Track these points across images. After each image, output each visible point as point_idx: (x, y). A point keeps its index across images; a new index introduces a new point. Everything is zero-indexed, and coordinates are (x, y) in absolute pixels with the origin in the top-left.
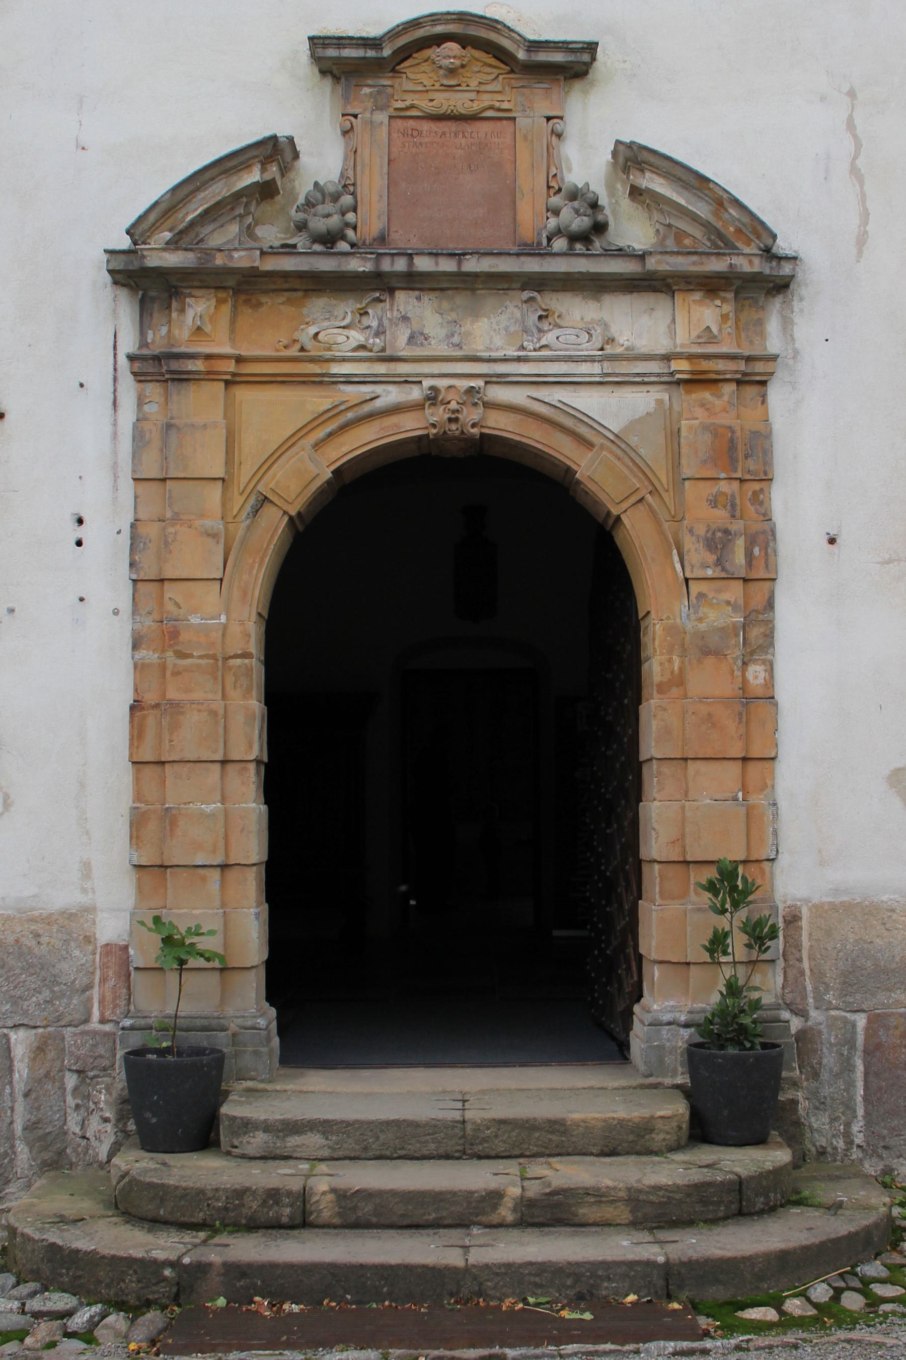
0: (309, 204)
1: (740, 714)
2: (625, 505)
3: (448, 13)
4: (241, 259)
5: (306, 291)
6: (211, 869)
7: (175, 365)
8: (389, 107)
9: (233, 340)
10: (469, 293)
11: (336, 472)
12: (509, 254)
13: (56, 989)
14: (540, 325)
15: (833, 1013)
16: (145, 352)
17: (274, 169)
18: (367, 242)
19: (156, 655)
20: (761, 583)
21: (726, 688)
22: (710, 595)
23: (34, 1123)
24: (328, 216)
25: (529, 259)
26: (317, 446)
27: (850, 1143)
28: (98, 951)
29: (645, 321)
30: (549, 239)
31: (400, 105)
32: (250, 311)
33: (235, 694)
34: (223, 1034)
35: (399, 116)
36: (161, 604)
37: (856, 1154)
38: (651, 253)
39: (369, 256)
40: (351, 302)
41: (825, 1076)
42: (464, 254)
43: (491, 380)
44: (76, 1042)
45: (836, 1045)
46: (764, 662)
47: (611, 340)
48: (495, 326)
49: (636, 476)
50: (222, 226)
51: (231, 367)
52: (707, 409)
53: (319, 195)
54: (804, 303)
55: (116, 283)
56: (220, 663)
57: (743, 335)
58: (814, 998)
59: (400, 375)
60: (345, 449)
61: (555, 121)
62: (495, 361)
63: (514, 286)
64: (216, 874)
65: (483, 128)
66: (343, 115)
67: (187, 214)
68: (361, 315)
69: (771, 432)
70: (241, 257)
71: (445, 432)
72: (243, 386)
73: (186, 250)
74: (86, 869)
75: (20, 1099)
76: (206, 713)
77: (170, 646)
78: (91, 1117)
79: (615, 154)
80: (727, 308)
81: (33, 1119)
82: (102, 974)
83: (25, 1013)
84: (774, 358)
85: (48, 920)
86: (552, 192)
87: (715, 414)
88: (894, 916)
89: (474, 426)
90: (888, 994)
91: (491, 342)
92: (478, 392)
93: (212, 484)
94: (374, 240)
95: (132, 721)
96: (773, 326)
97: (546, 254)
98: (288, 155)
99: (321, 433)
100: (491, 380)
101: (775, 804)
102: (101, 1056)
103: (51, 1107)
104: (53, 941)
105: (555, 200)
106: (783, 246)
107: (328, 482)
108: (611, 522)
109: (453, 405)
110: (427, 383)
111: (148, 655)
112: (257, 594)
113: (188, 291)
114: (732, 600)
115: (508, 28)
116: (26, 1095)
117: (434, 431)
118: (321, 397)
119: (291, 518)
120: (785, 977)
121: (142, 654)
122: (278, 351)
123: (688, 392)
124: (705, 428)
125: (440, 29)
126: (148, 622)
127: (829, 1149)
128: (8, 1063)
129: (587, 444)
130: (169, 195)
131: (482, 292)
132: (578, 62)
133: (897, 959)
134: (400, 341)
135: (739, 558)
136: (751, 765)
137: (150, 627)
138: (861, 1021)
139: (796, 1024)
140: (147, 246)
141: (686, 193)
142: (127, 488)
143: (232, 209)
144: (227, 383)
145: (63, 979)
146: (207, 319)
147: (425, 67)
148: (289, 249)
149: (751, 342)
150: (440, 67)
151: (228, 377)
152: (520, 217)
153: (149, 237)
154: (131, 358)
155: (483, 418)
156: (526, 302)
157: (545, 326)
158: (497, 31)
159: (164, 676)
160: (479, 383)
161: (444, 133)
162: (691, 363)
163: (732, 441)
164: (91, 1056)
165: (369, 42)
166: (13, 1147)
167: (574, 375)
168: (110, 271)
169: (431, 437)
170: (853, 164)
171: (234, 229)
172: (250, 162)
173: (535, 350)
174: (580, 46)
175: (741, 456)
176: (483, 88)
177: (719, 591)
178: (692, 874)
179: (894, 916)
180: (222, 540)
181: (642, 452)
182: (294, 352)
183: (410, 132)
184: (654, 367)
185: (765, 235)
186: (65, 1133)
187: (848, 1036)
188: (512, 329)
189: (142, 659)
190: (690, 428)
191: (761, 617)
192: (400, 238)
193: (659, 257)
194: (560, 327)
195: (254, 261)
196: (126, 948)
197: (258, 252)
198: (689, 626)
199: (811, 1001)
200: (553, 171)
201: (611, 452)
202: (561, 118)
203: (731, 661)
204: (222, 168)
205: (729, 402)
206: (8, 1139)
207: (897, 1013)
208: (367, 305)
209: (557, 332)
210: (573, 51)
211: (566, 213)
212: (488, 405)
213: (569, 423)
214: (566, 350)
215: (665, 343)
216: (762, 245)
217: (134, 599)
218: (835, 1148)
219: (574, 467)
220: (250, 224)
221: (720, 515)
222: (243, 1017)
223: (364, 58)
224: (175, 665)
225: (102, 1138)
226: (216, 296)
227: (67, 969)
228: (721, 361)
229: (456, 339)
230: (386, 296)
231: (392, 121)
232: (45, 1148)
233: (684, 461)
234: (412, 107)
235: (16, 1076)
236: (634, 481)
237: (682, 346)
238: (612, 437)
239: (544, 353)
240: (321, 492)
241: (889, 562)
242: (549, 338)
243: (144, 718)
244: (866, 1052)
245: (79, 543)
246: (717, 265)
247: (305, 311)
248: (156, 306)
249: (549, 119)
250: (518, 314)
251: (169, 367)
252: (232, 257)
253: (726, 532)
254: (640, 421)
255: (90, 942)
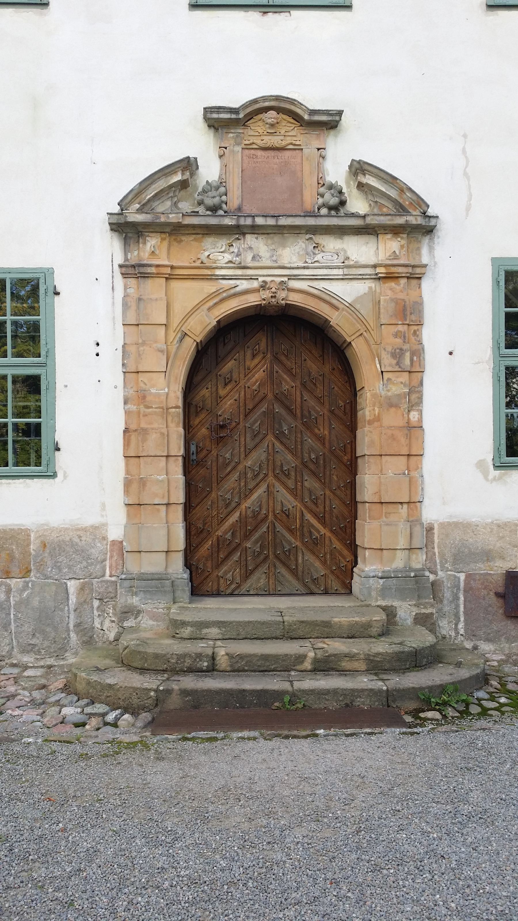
0: (204, 191)
1: (407, 435)
2: (353, 337)
3: (271, 96)
4: (173, 218)
5: (203, 234)
6: (162, 506)
7: (142, 270)
8: (242, 143)
9: (168, 258)
10: (280, 235)
11: (218, 322)
12: (301, 216)
13: (89, 561)
14: (314, 251)
15: (449, 573)
16: (127, 263)
17: (188, 174)
18: (232, 211)
19: (135, 407)
20: (417, 373)
21: (401, 423)
22: (393, 379)
23: (79, 624)
24: (214, 197)
25: (310, 218)
26: (209, 309)
27: (457, 633)
28: (109, 543)
29: (364, 248)
30: (319, 209)
31: (247, 142)
32: (177, 244)
33: (172, 425)
34: (167, 581)
35: (247, 148)
36: (137, 383)
37: (460, 638)
38: (368, 215)
39: (234, 217)
40: (225, 240)
41: (445, 602)
42: (279, 216)
43: (291, 277)
44: (98, 585)
45: (450, 588)
46: (418, 410)
47: (348, 258)
48: (293, 252)
49: (359, 323)
50: (163, 202)
51: (168, 270)
52: (393, 291)
53: (209, 187)
54: (440, 239)
55: (112, 230)
56: (165, 411)
57: (411, 255)
58: (440, 566)
59: (248, 276)
60: (222, 311)
61: (322, 150)
62: (293, 268)
63: (302, 232)
64: (164, 508)
65: (287, 154)
66: (220, 148)
67: (147, 195)
68: (229, 246)
69: (423, 302)
70: (173, 217)
71: (269, 303)
72: (173, 280)
73: (146, 213)
74: (103, 506)
75: (72, 612)
76: (159, 434)
77: (142, 403)
78: (105, 620)
79: (350, 167)
80: (403, 242)
81: (79, 621)
82: (111, 554)
83: (75, 573)
84: (425, 266)
85: (85, 530)
86: (320, 185)
87: (397, 293)
88: (478, 528)
89: (283, 300)
90: (475, 564)
91: (291, 259)
92: (285, 284)
93: (160, 326)
94: (235, 210)
95: (124, 438)
96: (425, 251)
97: (318, 216)
98: (194, 168)
99: (211, 303)
100: (291, 277)
101: (422, 476)
102: (110, 592)
103: (87, 616)
104: (87, 539)
105: (322, 190)
106: (431, 212)
107: (214, 327)
108: (345, 345)
109: (273, 290)
110: (261, 279)
111: (132, 407)
112: (182, 379)
113: (147, 234)
114: (404, 382)
115: (300, 103)
116: (75, 611)
117: (264, 302)
118: (210, 286)
119: (197, 343)
120: (427, 557)
121: (129, 406)
122: (190, 263)
123: (384, 283)
124: (392, 300)
125: (267, 104)
126: (131, 392)
127: (448, 636)
128: (67, 596)
129: (337, 308)
130: (138, 186)
131: (287, 235)
132: (333, 121)
133: (480, 548)
134: (248, 258)
135: (407, 361)
136: (412, 458)
137: (132, 394)
138: (462, 576)
139: (432, 577)
140: (128, 211)
141: (385, 185)
142: (120, 329)
143: (168, 194)
144: (167, 278)
145: (92, 557)
146: (156, 247)
147: (260, 123)
148: (195, 214)
149: (414, 259)
150: (267, 123)
151: (167, 276)
152: (305, 198)
153: (129, 207)
154: (121, 266)
155: (287, 296)
156: (307, 240)
157: (317, 251)
158: (293, 104)
159: (139, 417)
160: (285, 279)
161: (268, 157)
162: (386, 269)
163: (405, 306)
164: (105, 592)
165: (233, 110)
166: (69, 635)
167: (330, 275)
168: (110, 224)
169: (262, 305)
170: (465, 170)
171: (168, 203)
172: (177, 170)
173: (312, 263)
174: (335, 112)
175: (408, 313)
176: (287, 134)
177: (397, 377)
178: (384, 508)
179: (478, 528)
180: (166, 353)
181: (362, 312)
182: (198, 264)
183: (252, 156)
184: (369, 271)
185: (423, 206)
186: (94, 628)
187: (456, 583)
188: (301, 253)
189: (129, 409)
190: (385, 300)
191: (417, 389)
192: (247, 209)
193: (372, 217)
194: (324, 252)
195: (179, 219)
196: (122, 542)
197: (181, 215)
198: (383, 393)
199: (439, 567)
200: (321, 175)
201: (347, 312)
202: (324, 149)
203: (403, 410)
204: (163, 173)
205: (403, 288)
206: (66, 631)
207: (479, 573)
208: (232, 241)
209: (322, 254)
210: (331, 115)
211: (327, 196)
212: (290, 290)
213: (327, 298)
214: (327, 263)
215: (373, 259)
216: (422, 211)
217: (124, 381)
218: (450, 636)
219: (329, 319)
220: (176, 202)
221: (399, 341)
222: (177, 573)
223: (230, 119)
224: (144, 412)
225: (111, 630)
226: (160, 236)
227: (95, 552)
228: (400, 268)
229: (274, 258)
230: (241, 237)
231: (243, 150)
232: (84, 635)
233: (382, 316)
234: (253, 143)
235: (70, 602)
236: (358, 325)
237: (382, 260)
238: (347, 305)
239: (316, 264)
240: (211, 331)
241: (479, 363)
242: (318, 257)
243: (130, 436)
244: (465, 591)
245: (97, 355)
246: (400, 221)
247: (203, 244)
248: (132, 241)
249: (318, 149)
250: (304, 245)
251: (139, 270)
252: (168, 217)
253: (401, 349)
254: (361, 297)
255: (105, 539)
